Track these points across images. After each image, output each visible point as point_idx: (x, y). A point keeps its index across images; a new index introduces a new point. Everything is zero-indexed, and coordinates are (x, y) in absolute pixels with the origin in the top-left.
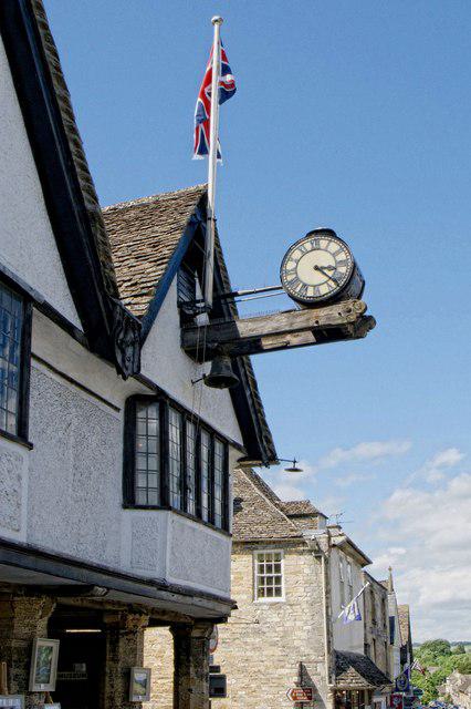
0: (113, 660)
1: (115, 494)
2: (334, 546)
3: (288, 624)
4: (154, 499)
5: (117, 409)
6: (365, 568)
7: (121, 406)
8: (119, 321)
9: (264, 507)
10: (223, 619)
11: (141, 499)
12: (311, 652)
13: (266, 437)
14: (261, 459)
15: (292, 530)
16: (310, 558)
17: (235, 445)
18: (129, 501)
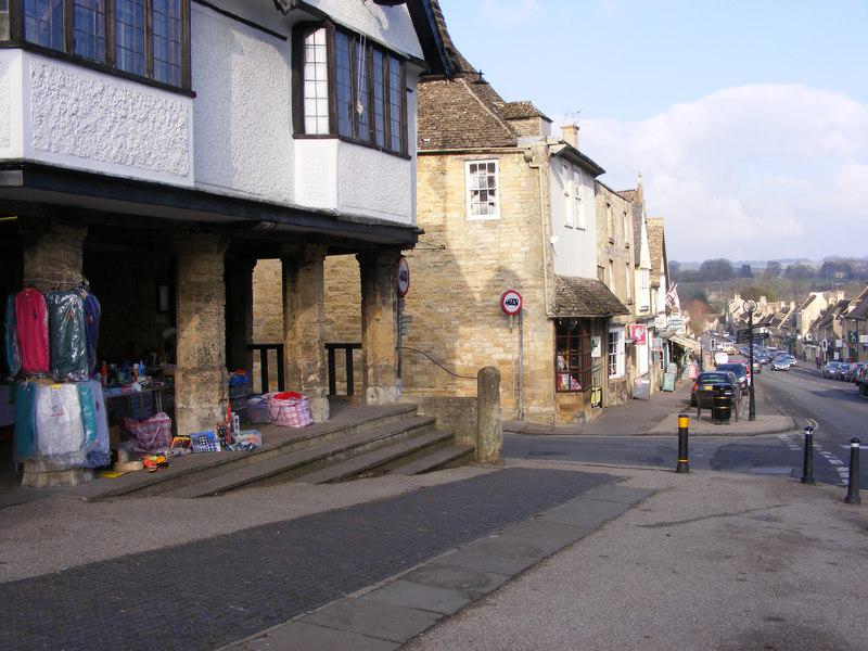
0: (293, 290)
1: (289, 129)
2: (553, 155)
3: (503, 245)
4: (324, 128)
5: (284, 39)
6: (598, 178)
7: (289, 35)
8: (163, 454)
9: (440, 147)
10: (410, 245)
11: (310, 128)
12: (530, 276)
13: (448, 49)
14: (444, 72)
15: (265, 635)
16: (523, 164)
17: (413, 59)
18: (299, 131)
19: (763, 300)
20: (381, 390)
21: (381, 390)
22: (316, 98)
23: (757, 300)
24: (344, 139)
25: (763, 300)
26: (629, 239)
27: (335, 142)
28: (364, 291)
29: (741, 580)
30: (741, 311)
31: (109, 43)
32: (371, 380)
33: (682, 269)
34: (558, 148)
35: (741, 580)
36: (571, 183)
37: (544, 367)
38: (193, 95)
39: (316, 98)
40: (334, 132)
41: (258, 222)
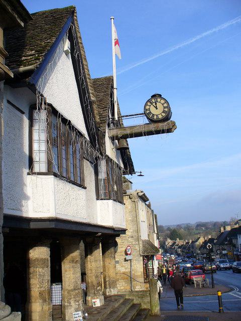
1: (95, 197)
19: (178, 239)
20: (112, 290)
21: (112, 290)
22: (39, 151)
23: (176, 240)
24: (55, 175)
25: (178, 239)
26: (152, 224)
27: (51, 178)
28: (103, 254)
29: (182, 283)
30: (170, 244)
31: (82, 180)
32: (108, 286)
33: (24, 202)
34: (141, 194)
35: (182, 283)
36: (141, 205)
37: (140, 274)
38: (85, 188)
39: (39, 151)
40: (49, 172)
41: (98, 233)
